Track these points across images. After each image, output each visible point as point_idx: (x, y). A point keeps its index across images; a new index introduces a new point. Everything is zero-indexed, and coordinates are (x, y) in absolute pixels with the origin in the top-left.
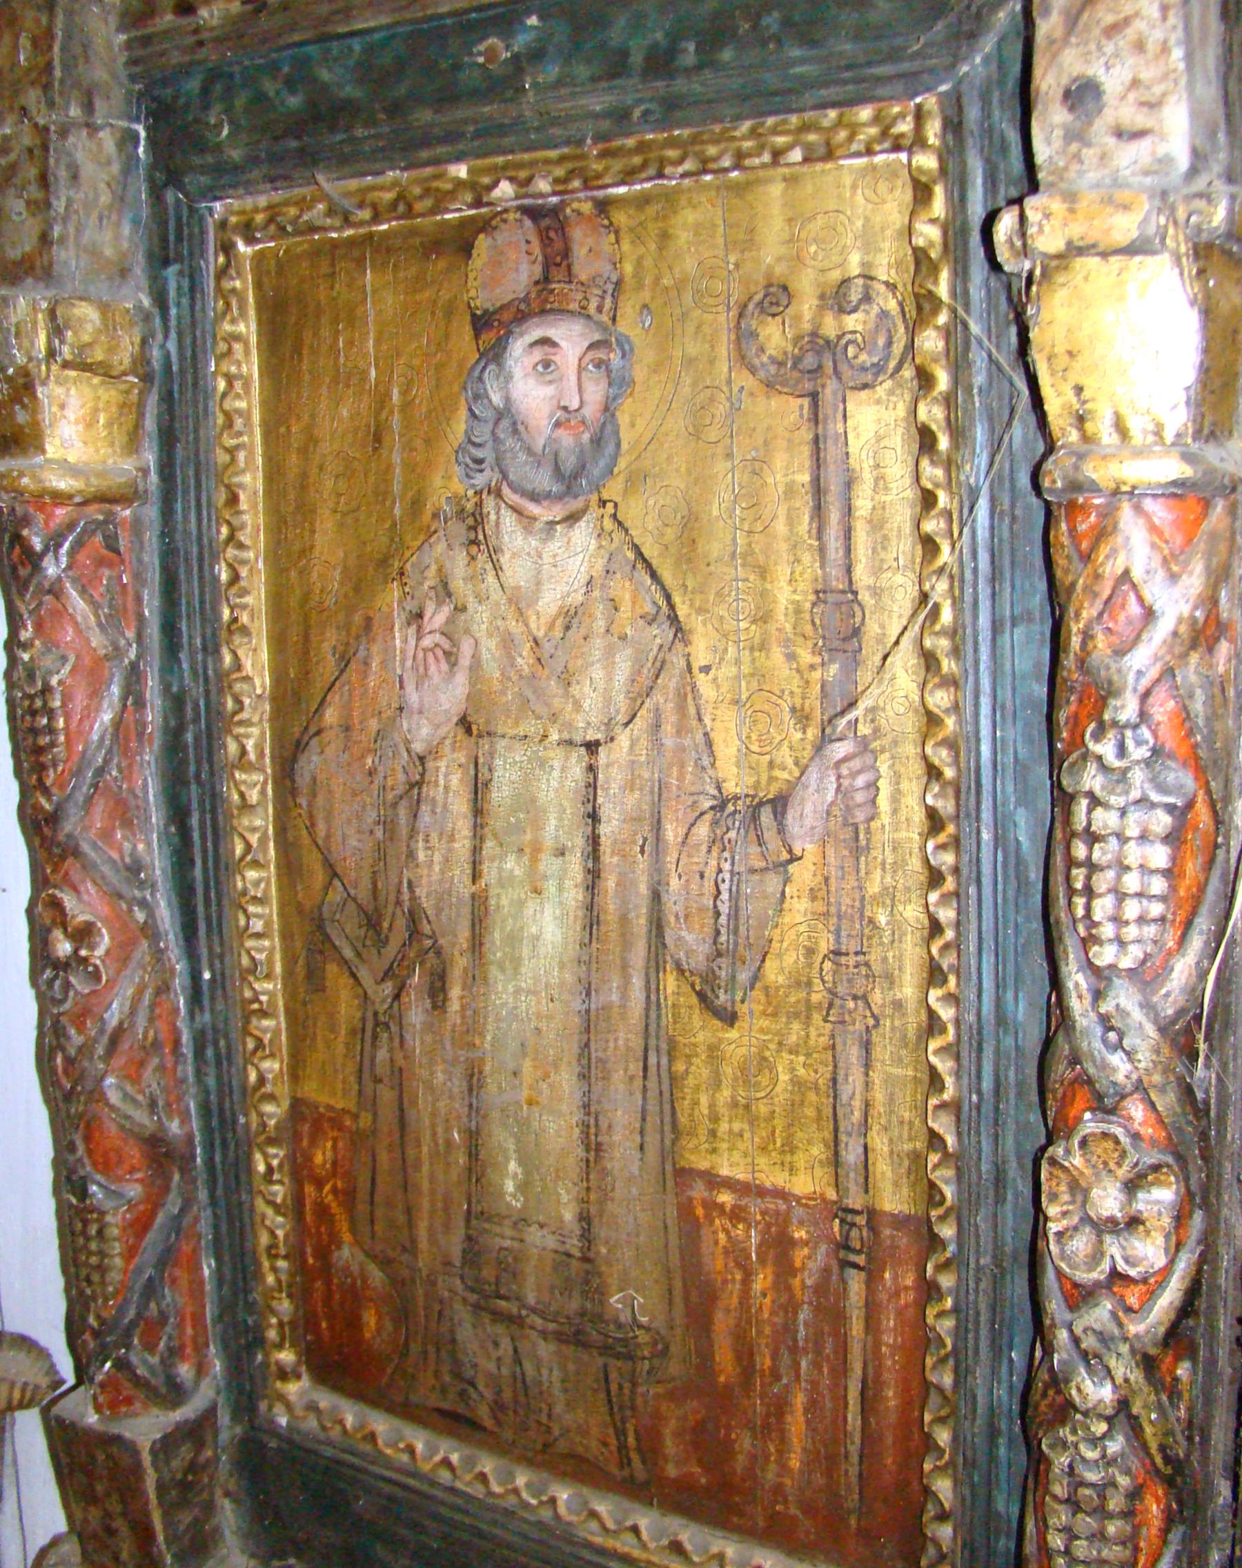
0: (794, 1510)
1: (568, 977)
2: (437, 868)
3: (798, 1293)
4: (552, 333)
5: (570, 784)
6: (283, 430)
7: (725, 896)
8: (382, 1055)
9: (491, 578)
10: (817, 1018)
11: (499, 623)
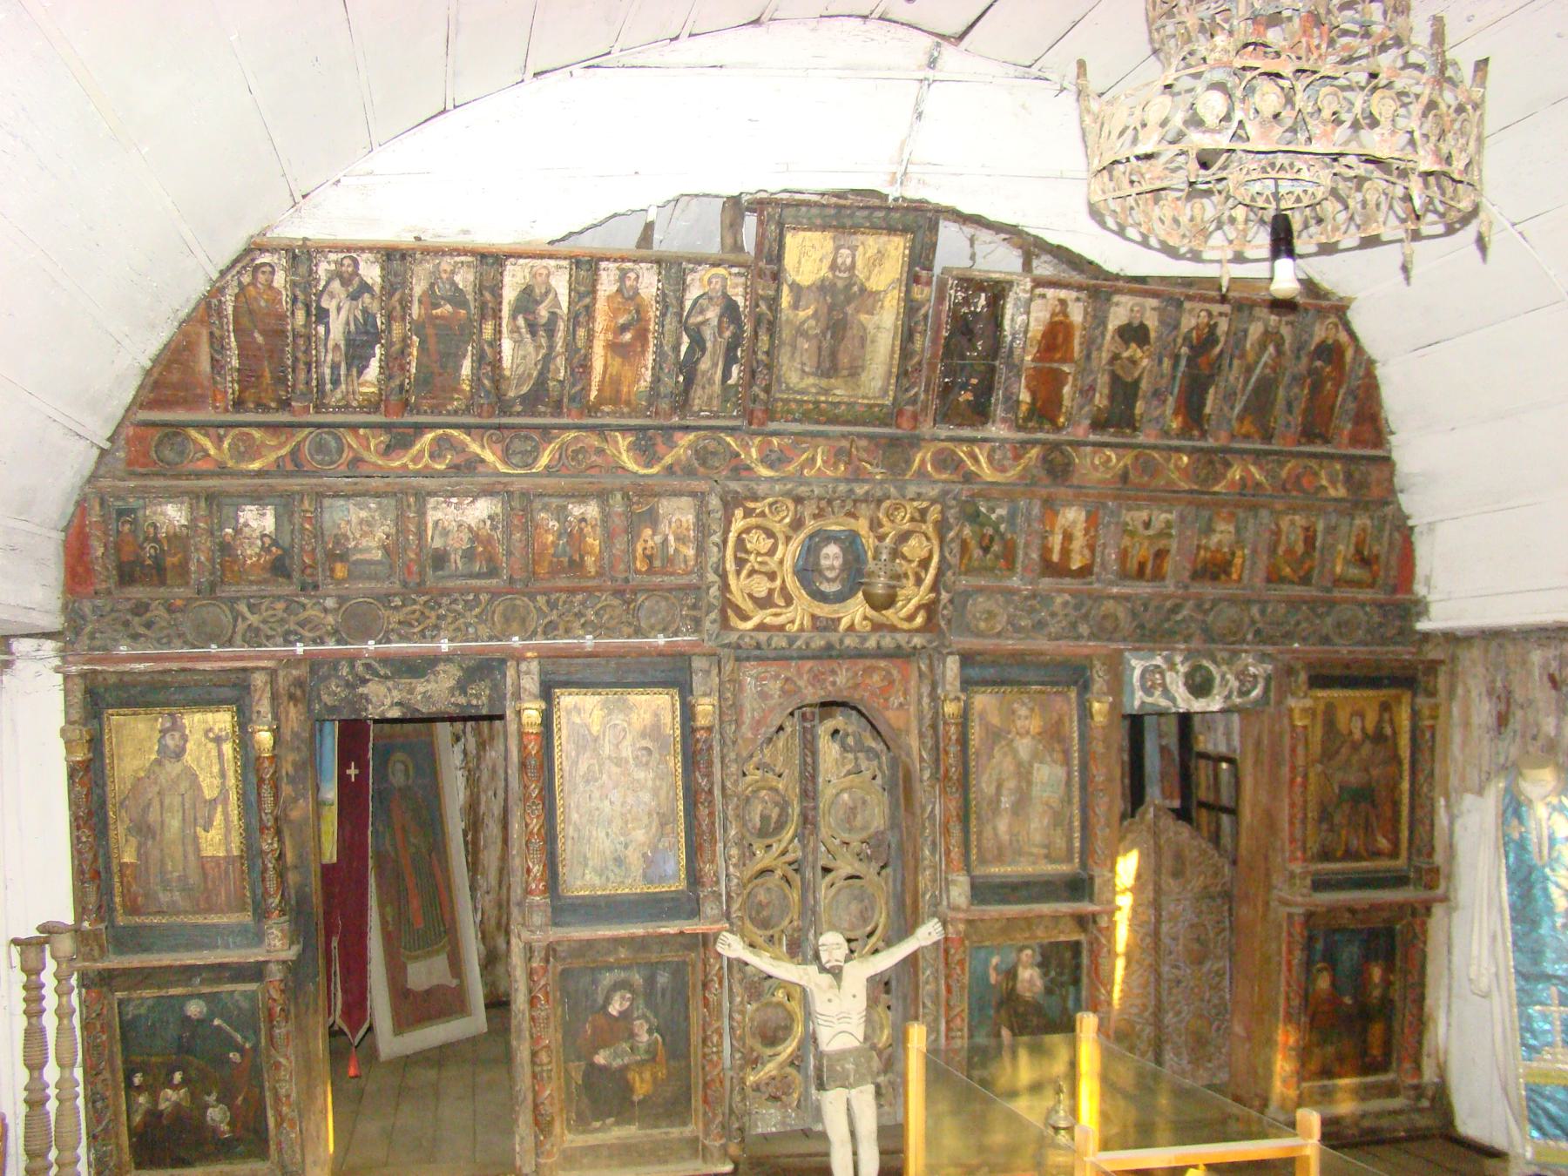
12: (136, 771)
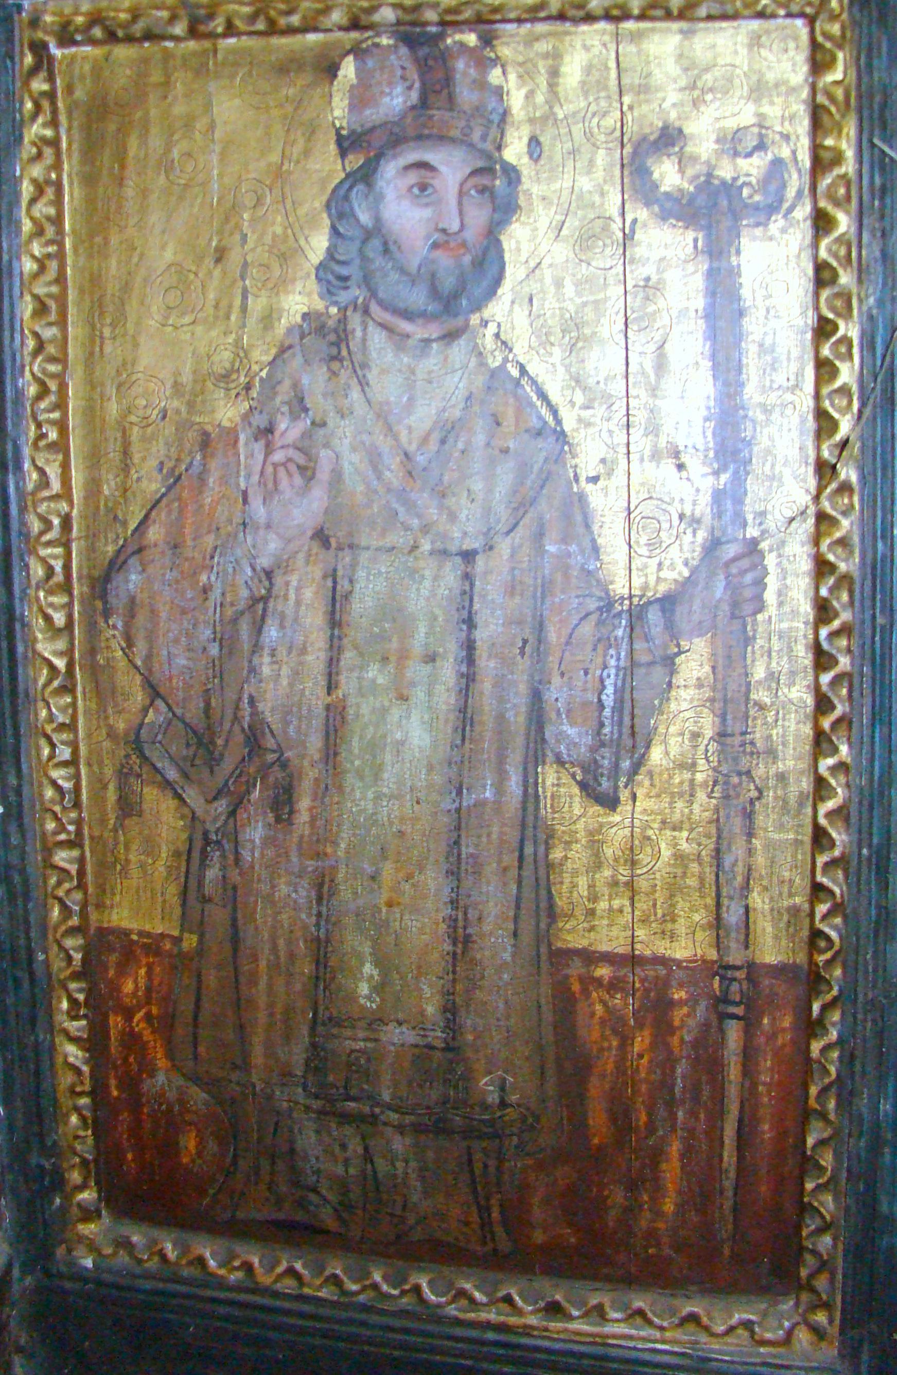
0: (667, 1251)
1: (437, 779)
2: (285, 682)
3: (676, 1051)
4: (430, 157)
5: (443, 591)
6: (98, 240)
7: (610, 690)
8: (212, 873)
9: (355, 394)
10: (701, 796)
11: (365, 437)
12: (194, 396)
